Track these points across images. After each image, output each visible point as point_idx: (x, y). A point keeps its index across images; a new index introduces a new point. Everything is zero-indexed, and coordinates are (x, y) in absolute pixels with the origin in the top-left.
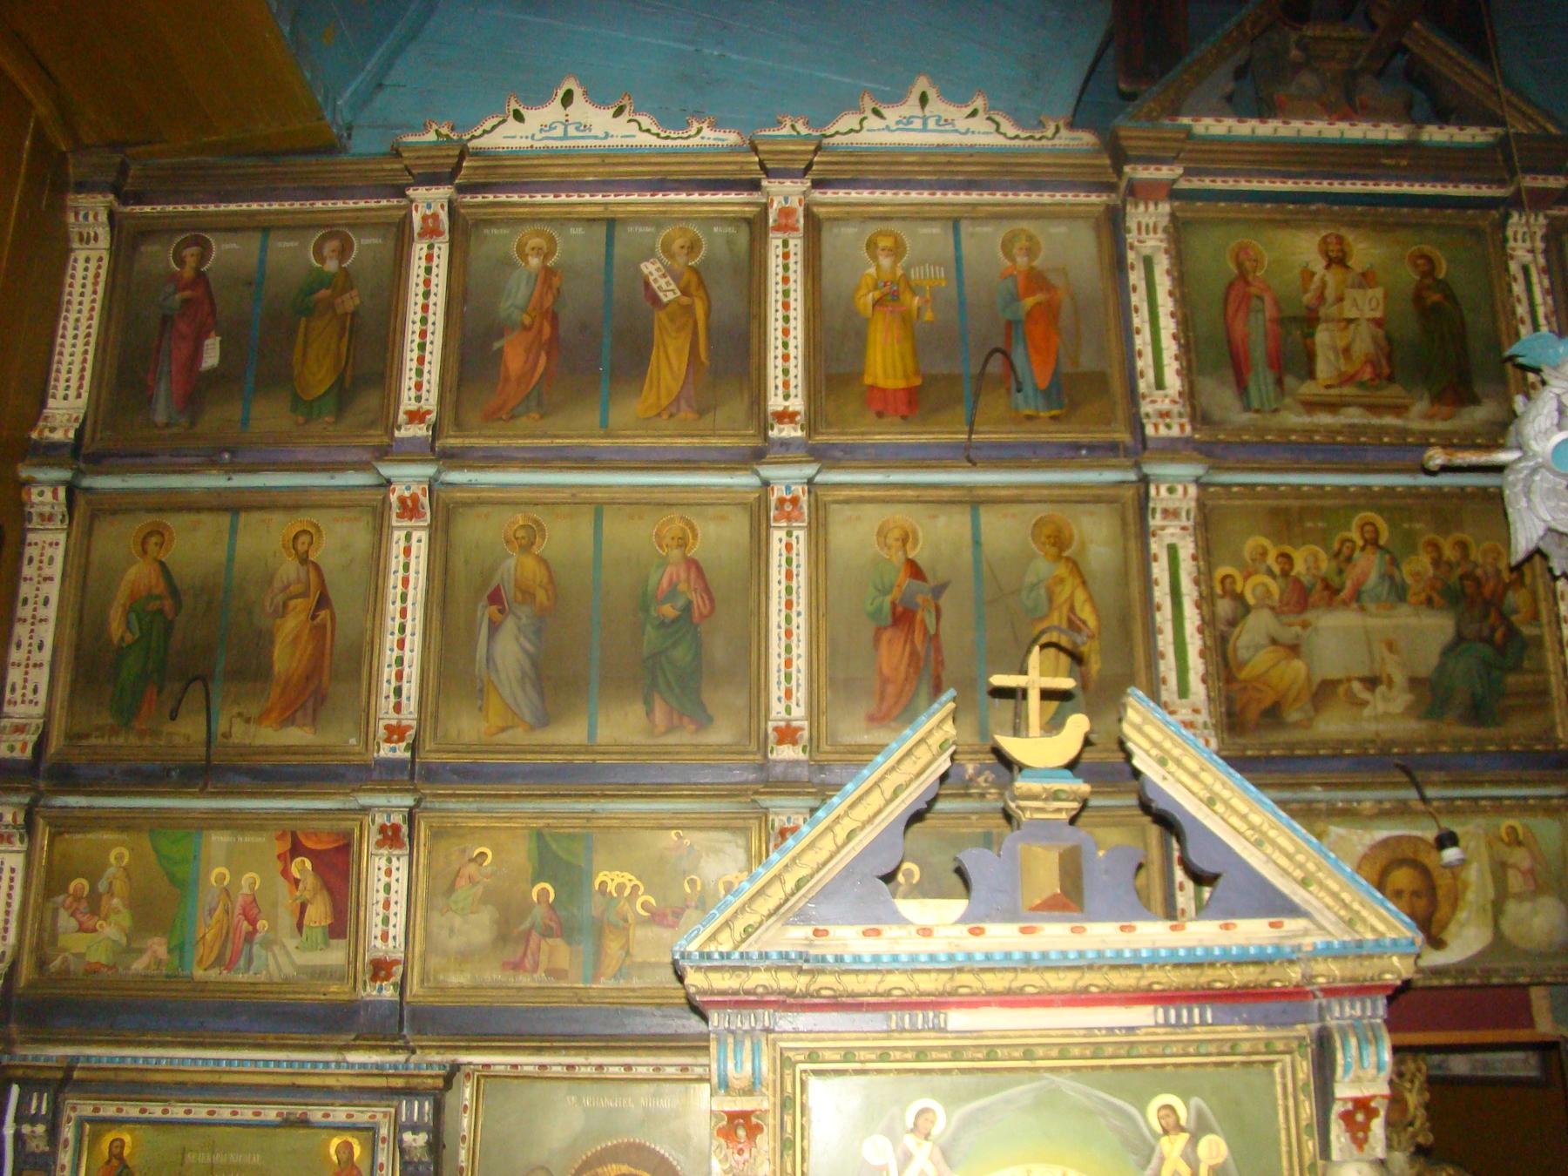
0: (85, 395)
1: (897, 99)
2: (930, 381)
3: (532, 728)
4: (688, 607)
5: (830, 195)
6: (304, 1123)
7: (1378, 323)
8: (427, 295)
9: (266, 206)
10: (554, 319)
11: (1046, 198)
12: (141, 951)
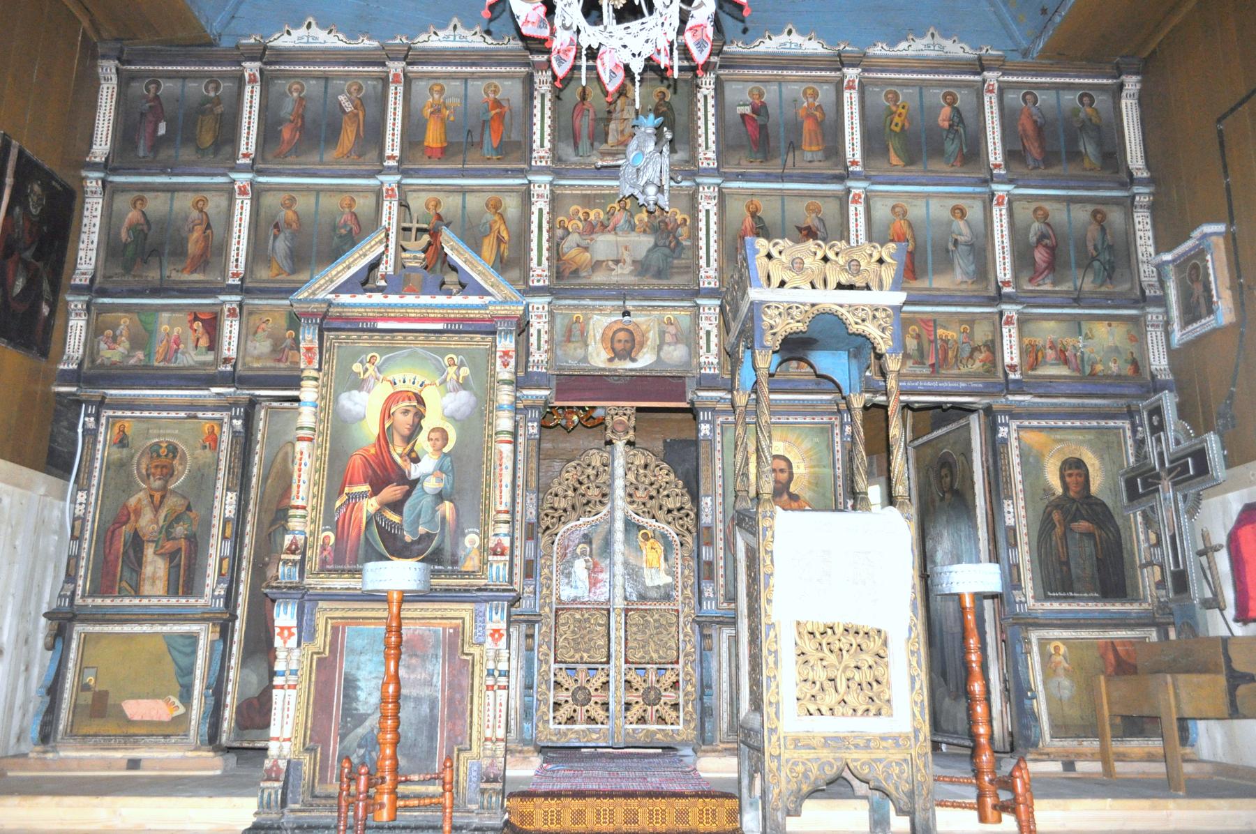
1: (444, 27)
2: (451, 144)
3: (289, 275)
5: (415, 68)
6: (196, 417)
8: (251, 107)
9: (184, 68)
10: (303, 118)
11: (503, 69)
12: (133, 356)
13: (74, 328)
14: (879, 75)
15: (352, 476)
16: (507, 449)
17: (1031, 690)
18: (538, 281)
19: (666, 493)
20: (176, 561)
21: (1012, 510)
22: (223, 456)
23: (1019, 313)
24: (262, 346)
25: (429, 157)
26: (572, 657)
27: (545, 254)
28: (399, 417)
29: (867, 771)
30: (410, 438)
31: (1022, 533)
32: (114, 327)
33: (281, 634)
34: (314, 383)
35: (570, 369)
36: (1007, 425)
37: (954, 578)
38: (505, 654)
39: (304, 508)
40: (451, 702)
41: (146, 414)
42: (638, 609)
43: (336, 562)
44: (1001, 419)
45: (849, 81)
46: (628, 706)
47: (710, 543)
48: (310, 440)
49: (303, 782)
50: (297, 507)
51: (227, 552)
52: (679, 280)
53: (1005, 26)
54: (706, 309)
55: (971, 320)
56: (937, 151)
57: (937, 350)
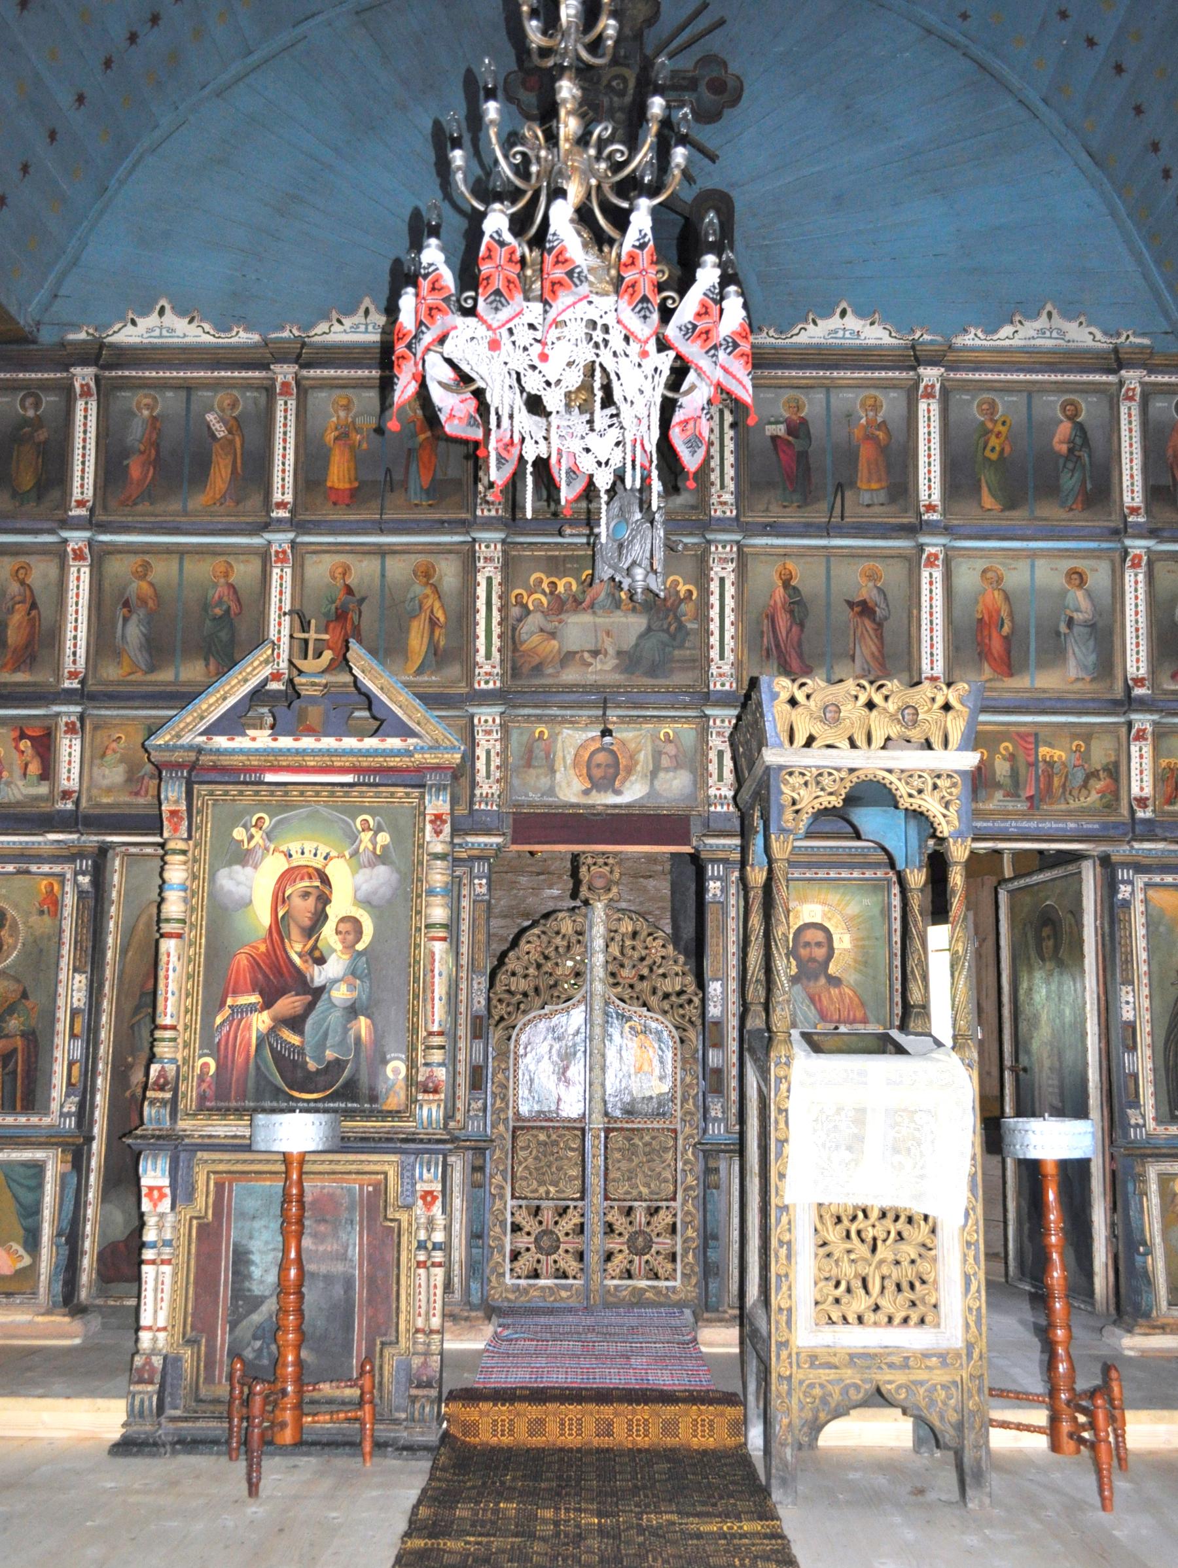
3: (146, 673)
5: (312, 373)
8: (85, 432)
14: (970, 376)
16: (439, 947)
17: (1144, 1244)
18: (487, 682)
19: (661, 971)
20: (11, 1066)
21: (1131, 1000)
22: (68, 925)
23: (1155, 724)
24: (114, 774)
25: (335, 504)
26: (536, 1191)
27: (496, 642)
28: (297, 901)
29: (903, 1396)
31: (1144, 1038)
33: (149, 1195)
34: (182, 858)
35: (530, 806)
36: (1130, 882)
37: (1031, 1139)
38: (440, 1220)
39: (174, 1028)
40: (371, 1281)
42: (622, 1129)
43: (218, 1098)
44: (1122, 874)
45: (926, 387)
46: (609, 1257)
47: (719, 1044)
48: (179, 936)
49: (183, 1383)
50: (165, 1028)
51: (77, 1054)
52: (681, 678)
53: (1158, 296)
54: (718, 722)
55: (1087, 734)
56: (1049, 489)
57: (1038, 780)
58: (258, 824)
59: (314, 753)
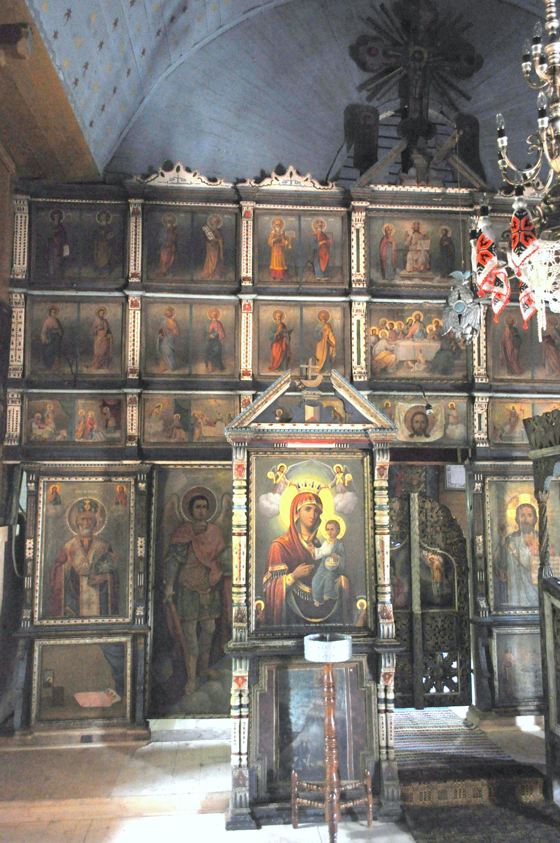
0: (26, 264)
4: (217, 336)
5: (261, 206)
7: (428, 251)
8: (136, 235)
12: (59, 434)
13: (12, 412)
15: (273, 558)
18: (360, 377)
20: (104, 590)
28: (304, 513)
30: (313, 529)
32: (43, 411)
41: (73, 479)
58: (281, 470)
59: (315, 432)
